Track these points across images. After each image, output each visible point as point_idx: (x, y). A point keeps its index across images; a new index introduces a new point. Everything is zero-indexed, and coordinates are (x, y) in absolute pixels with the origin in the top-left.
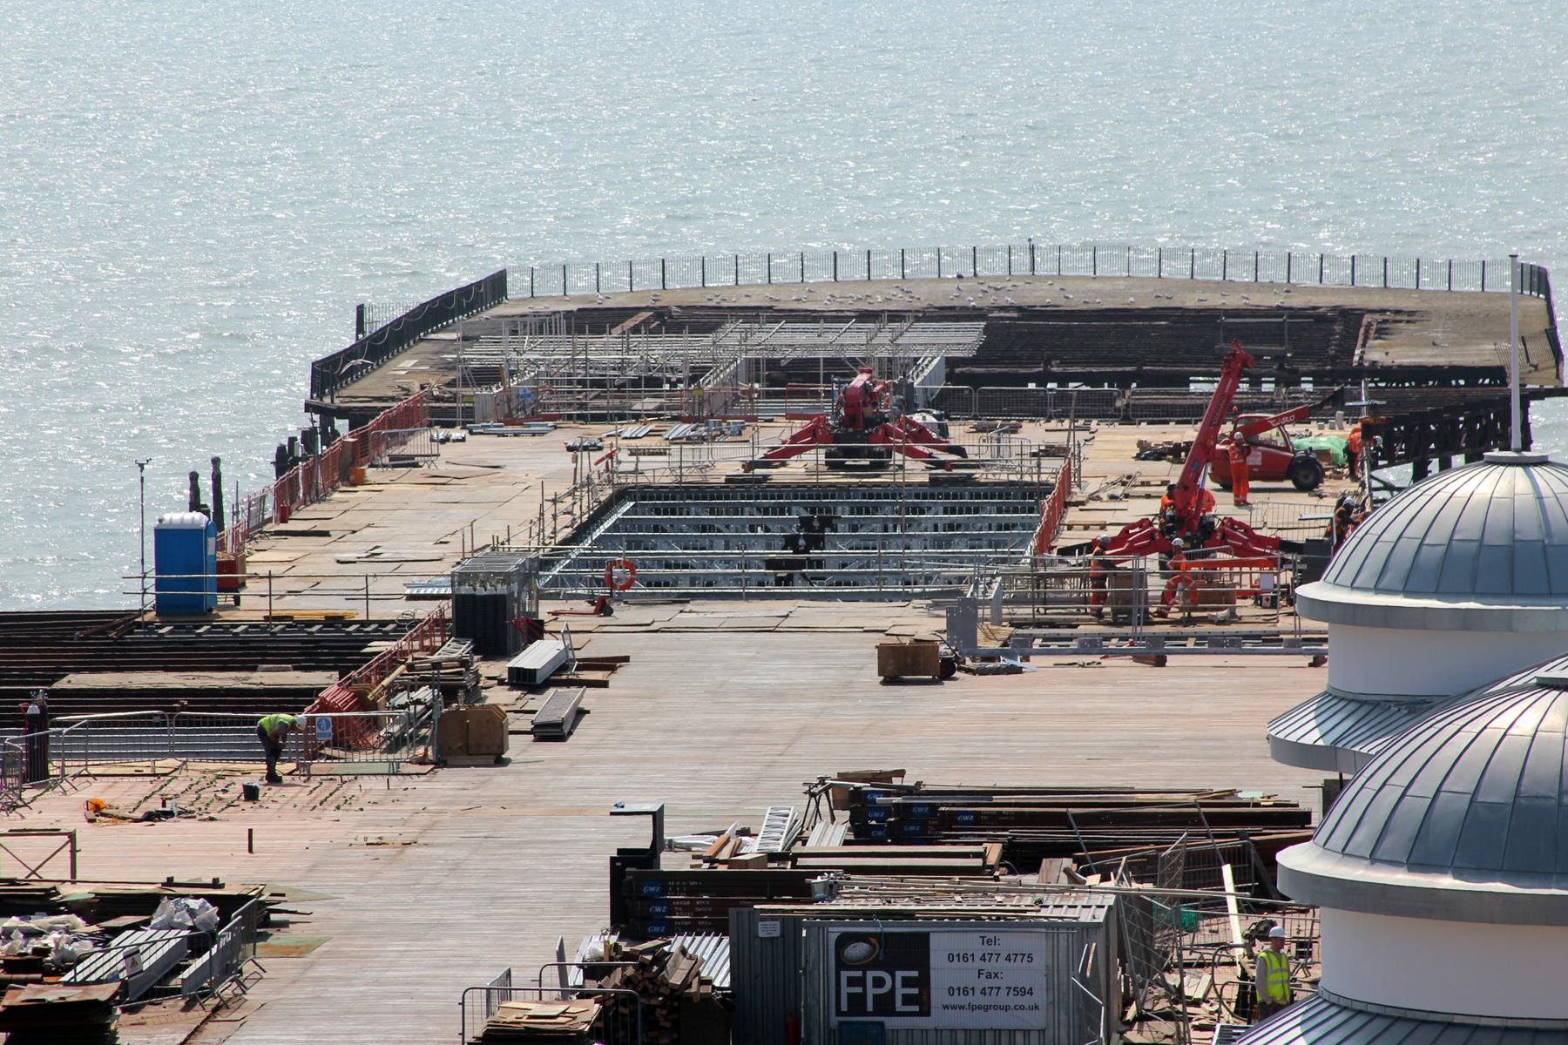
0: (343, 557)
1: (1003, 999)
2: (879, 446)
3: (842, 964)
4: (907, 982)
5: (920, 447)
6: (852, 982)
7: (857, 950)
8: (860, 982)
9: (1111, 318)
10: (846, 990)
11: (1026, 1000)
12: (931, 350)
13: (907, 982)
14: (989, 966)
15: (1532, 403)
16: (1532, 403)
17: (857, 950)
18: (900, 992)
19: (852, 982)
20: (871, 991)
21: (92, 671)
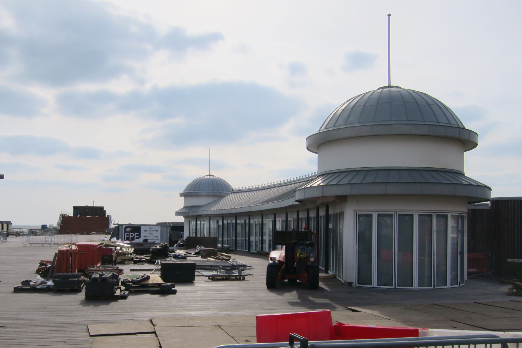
0: (478, 301)
1: (153, 238)
2: (114, 255)
3: (125, 232)
4: (137, 235)
5: (460, 220)
6: (127, 235)
7: (128, 229)
8: (129, 235)
9: (410, 195)
10: (126, 236)
11: (157, 238)
12: (26, 231)
13: (137, 235)
14: (151, 232)
15: (500, 344)
16: (500, 344)
17: (128, 229)
18: (135, 236)
19: (127, 235)
20: (130, 236)
21: (468, 264)
